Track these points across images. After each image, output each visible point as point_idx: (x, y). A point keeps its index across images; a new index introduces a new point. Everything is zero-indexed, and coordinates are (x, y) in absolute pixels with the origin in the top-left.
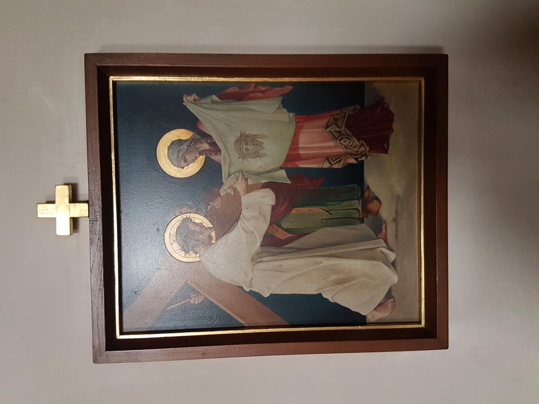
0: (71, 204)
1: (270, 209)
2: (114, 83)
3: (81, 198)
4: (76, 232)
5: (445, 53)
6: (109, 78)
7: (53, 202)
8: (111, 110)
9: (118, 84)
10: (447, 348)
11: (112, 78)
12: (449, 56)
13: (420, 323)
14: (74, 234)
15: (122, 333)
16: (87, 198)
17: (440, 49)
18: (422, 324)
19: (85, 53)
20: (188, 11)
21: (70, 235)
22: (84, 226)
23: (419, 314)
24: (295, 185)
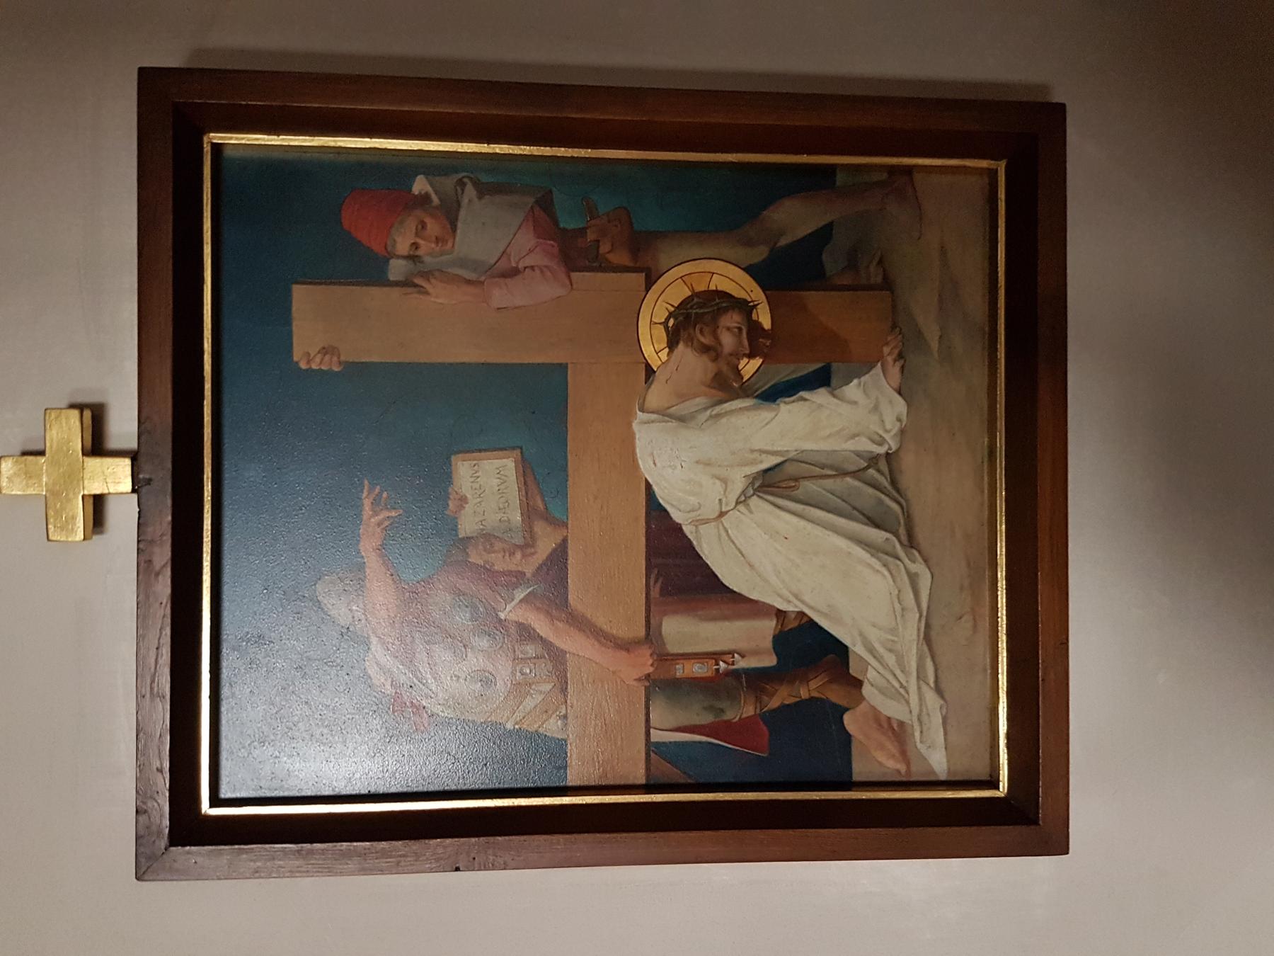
0: (87, 459)
1: (225, 859)
2: (217, 148)
3: (113, 443)
4: (101, 532)
5: (1057, 98)
6: (202, 132)
7: (41, 453)
8: (205, 220)
9: (228, 153)
10: (1068, 853)
11: (217, 137)
12: (1068, 108)
13: (995, 786)
14: (95, 537)
15: (216, 801)
16: (133, 445)
17: (1044, 88)
18: (1001, 790)
19: (139, 66)
20: (786, 538)
21: (84, 539)
22: (123, 516)
23: (991, 754)
24: (424, 687)
